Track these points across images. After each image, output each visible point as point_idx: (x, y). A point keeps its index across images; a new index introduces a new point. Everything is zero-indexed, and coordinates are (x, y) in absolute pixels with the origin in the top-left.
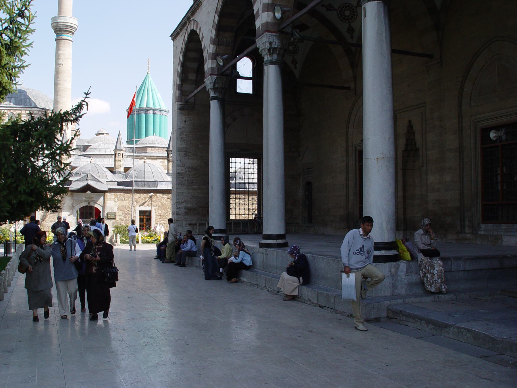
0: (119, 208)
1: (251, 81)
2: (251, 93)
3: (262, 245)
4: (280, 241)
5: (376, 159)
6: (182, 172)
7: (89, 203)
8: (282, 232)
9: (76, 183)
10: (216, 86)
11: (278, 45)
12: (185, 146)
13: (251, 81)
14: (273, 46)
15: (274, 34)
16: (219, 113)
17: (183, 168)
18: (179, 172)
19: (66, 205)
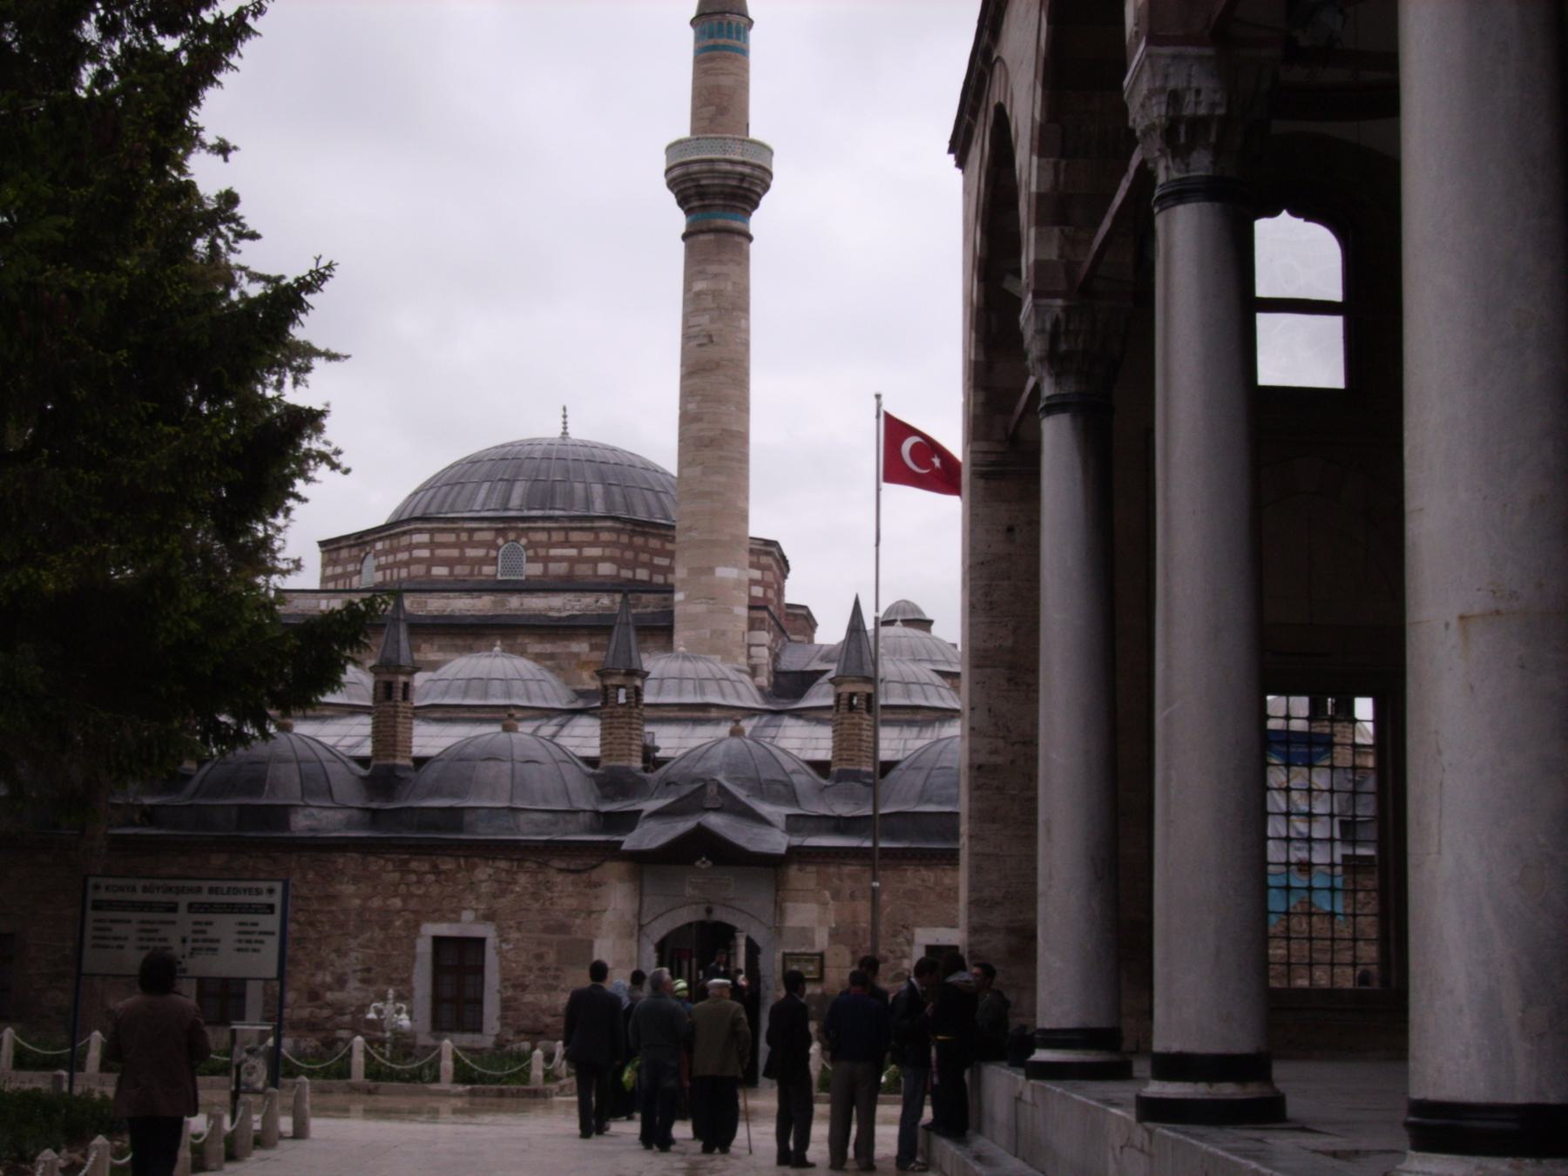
0: (835, 936)
1: (1336, 323)
2: (1339, 383)
3: (1152, 1110)
4: (1227, 1090)
5: (1454, 623)
6: (999, 759)
7: (709, 911)
8: (1242, 1042)
9: (651, 825)
10: (1063, 347)
11: (1213, 105)
12: (1009, 643)
13: (1336, 323)
14: (1188, 111)
15: (1191, 51)
16: (1078, 474)
17: (1001, 743)
18: (982, 758)
19: (609, 917)
